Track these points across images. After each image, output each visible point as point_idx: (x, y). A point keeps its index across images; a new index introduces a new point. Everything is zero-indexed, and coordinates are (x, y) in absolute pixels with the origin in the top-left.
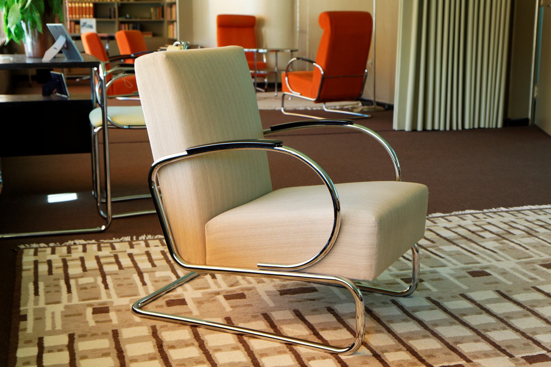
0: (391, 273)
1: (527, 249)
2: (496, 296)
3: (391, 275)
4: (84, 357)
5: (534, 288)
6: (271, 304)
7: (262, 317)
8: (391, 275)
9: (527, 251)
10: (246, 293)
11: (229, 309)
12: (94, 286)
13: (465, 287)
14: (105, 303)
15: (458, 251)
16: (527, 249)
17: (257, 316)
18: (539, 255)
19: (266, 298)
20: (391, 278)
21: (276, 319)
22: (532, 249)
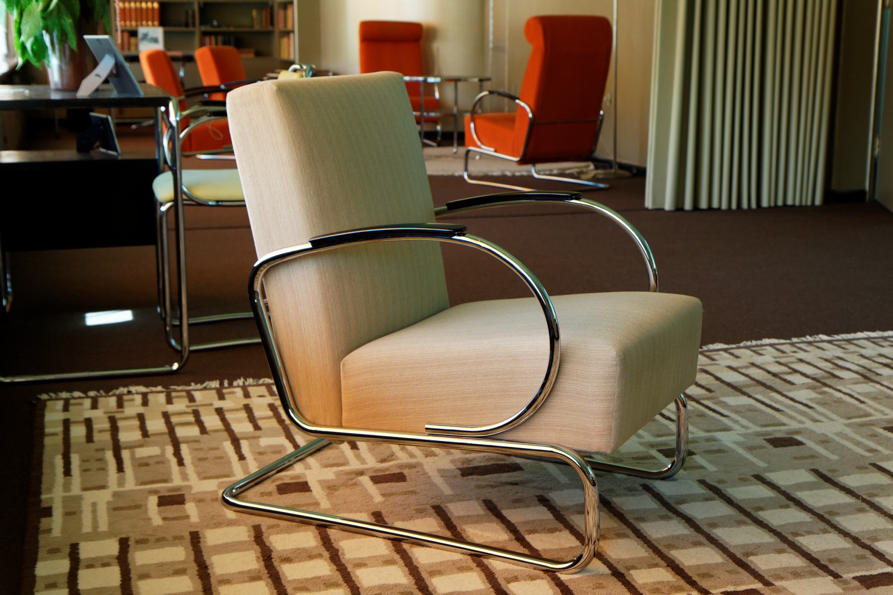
0: (642, 440)
1: (862, 402)
2: (811, 478)
3: (641, 444)
4: (145, 576)
5: (875, 465)
6: (762, 464)
7: (432, 511)
8: (641, 444)
9: (862, 406)
10: (406, 472)
11: (378, 499)
12: (161, 461)
13: (762, 464)
14: (178, 489)
15: (750, 405)
16: (862, 402)
17: (425, 510)
18: (882, 412)
19: (438, 480)
20: (641, 449)
21: (456, 514)
22: (871, 402)
